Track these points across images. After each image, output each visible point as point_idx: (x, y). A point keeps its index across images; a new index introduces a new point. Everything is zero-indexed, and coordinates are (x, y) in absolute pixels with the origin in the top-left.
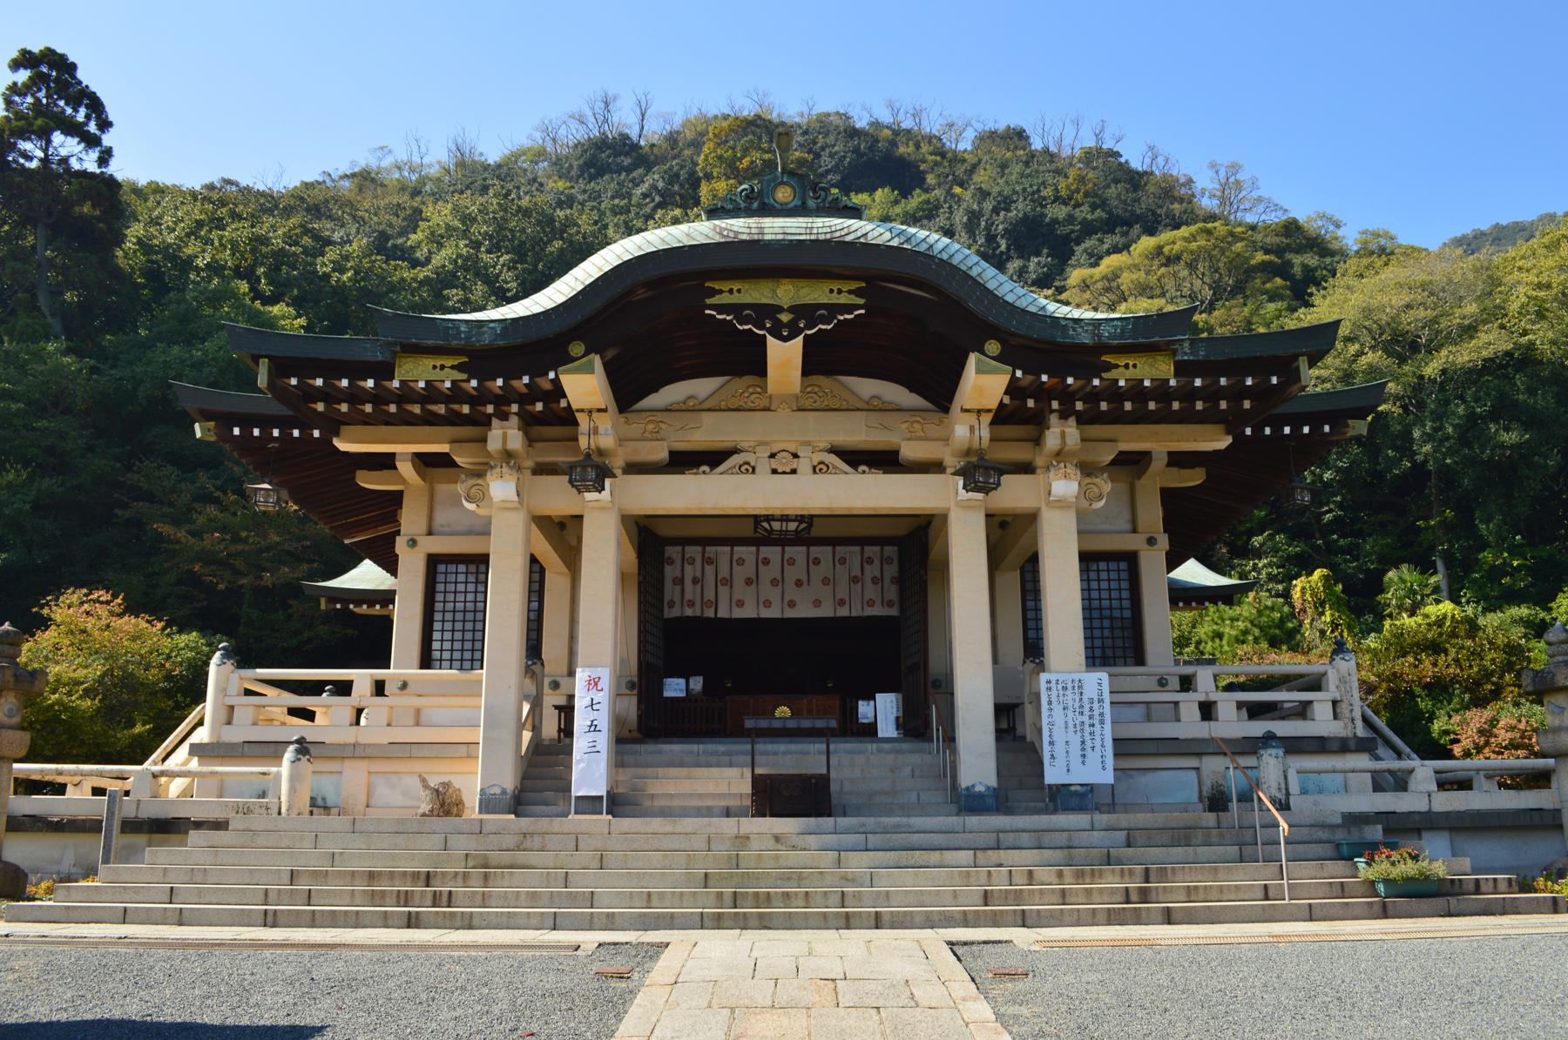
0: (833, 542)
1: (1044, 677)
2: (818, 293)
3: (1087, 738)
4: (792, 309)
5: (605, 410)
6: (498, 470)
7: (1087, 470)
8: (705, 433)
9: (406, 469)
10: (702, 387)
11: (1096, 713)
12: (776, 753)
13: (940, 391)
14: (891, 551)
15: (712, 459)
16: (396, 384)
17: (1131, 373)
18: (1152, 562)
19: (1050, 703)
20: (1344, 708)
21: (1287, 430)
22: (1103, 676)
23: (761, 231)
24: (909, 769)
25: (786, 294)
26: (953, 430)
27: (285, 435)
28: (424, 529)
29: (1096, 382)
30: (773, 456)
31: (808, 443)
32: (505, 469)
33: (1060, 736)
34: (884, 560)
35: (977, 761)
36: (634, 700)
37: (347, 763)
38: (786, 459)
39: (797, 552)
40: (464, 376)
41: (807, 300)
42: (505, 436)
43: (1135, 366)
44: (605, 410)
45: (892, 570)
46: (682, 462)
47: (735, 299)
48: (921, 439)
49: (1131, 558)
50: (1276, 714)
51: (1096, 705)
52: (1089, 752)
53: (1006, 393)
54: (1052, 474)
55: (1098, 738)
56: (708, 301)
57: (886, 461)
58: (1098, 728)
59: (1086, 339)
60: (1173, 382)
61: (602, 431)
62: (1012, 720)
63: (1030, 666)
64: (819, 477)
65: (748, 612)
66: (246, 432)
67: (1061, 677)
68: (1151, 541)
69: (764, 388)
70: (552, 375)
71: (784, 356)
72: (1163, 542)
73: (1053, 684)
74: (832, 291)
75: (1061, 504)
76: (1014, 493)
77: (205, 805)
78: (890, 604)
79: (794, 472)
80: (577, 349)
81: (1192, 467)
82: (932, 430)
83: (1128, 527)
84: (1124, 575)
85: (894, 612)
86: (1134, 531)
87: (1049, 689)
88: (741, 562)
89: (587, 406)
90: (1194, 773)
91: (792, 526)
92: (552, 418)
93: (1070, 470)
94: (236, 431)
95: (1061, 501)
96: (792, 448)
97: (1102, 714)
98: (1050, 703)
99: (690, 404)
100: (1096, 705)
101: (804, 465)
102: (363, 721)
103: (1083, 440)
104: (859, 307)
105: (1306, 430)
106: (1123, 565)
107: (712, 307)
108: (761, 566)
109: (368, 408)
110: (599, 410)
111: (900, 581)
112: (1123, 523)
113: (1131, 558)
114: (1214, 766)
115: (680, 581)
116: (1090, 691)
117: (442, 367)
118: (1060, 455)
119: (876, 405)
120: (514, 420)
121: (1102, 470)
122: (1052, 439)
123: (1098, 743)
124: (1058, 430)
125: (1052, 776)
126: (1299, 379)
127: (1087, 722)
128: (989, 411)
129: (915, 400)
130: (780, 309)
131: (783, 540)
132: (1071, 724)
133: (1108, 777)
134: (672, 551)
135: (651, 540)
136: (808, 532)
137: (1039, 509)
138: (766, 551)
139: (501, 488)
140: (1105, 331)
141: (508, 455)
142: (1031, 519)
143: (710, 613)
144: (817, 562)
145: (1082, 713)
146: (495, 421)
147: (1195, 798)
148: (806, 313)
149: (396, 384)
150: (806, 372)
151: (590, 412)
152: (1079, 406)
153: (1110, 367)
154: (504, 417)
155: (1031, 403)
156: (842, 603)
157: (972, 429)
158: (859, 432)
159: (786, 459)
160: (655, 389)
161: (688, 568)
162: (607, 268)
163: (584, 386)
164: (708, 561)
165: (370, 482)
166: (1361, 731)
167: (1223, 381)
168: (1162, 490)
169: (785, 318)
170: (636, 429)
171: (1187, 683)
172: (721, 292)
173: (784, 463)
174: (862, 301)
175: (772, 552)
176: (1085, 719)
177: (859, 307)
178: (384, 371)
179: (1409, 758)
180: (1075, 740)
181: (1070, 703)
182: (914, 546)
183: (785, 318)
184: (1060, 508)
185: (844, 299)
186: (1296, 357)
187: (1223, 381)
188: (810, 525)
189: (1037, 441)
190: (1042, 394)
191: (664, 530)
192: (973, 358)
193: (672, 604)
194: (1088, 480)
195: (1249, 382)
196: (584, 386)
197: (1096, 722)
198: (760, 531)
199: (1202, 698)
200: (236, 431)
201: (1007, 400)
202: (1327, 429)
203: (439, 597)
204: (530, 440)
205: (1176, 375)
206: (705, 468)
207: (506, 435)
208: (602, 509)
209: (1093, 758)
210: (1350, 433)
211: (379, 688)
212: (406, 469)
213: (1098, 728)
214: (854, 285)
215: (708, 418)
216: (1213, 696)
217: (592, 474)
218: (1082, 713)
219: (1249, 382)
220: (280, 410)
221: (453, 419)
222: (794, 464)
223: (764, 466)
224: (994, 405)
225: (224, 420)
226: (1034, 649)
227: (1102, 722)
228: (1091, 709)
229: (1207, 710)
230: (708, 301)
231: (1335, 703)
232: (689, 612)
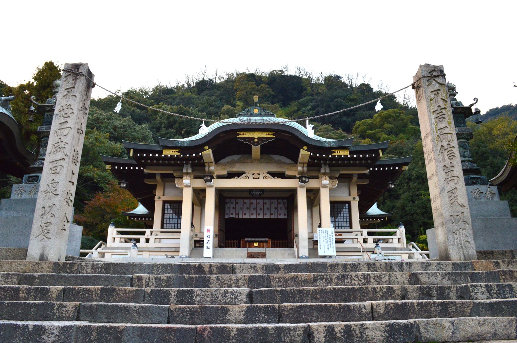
2: (264, 135)
4: (257, 138)
7: (331, 178)
8: (237, 168)
9: (158, 178)
10: (236, 157)
13: (294, 158)
14: (285, 201)
15: (238, 175)
16: (163, 156)
17: (339, 154)
20: (401, 240)
25: (256, 135)
27: (129, 168)
29: (330, 156)
34: (284, 204)
36: (217, 239)
41: (261, 136)
46: (231, 175)
57: (282, 176)
58: (332, 242)
59: (327, 145)
60: (349, 156)
62: (314, 244)
64: (265, 180)
66: (119, 168)
69: (251, 158)
71: (256, 150)
72: (357, 199)
75: (325, 186)
76: (313, 184)
78: (285, 215)
79: (258, 178)
80: (206, 147)
85: (286, 217)
86: (350, 196)
88: (246, 203)
91: (259, 193)
94: (116, 167)
96: (258, 172)
101: (261, 177)
109: (167, 162)
113: (349, 203)
115: (229, 208)
120: (190, 165)
121: (336, 178)
122: (322, 171)
123: (332, 246)
129: (292, 162)
130: (255, 138)
134: (227, 201)
135: (223, 197)
139: (186, 181)
140: (332, 144)
143: (237, 217)
144: (266, 203)
146: (185, 165)
149: (163, 156)
150: (261, 154)
151: (209, 163)
152: (328, 162)
154: (187, 164)
155: (316, 161)
156: (272, 214)
158: (275, 169)
160: (224, 158)
162: (214, 129)
163: (208, 153)
164: (236, 203)
165: (148, 182)
167: (361, 156)
169: (256, 140)
173: (256, 176)
175: (254, 201)
178: (160, 152)
180: (326, 245)
182: (289, 198)
183: (256, 140)
185: (270, 136)
187: (361, 156)
188: (263, 193)
189: (319, 171)
190: (319, 159)
191: (225, 195)
195: (367, 156)
200: (116, 167)
201: (310, 160)
202: (397, 168)
203: (166, 212)
205: (350, 154)
210: (403, 169)
211: (151, 232)
212: (158, 178)
214: (272, 133)
219: (157, 155)
220: (134, 162)
221: (175, 165)
223: (251, 176)
224: (307, 161)
225: (113, 165)
229: (365, 241)
231: (399, 239)
232: (231, 216)
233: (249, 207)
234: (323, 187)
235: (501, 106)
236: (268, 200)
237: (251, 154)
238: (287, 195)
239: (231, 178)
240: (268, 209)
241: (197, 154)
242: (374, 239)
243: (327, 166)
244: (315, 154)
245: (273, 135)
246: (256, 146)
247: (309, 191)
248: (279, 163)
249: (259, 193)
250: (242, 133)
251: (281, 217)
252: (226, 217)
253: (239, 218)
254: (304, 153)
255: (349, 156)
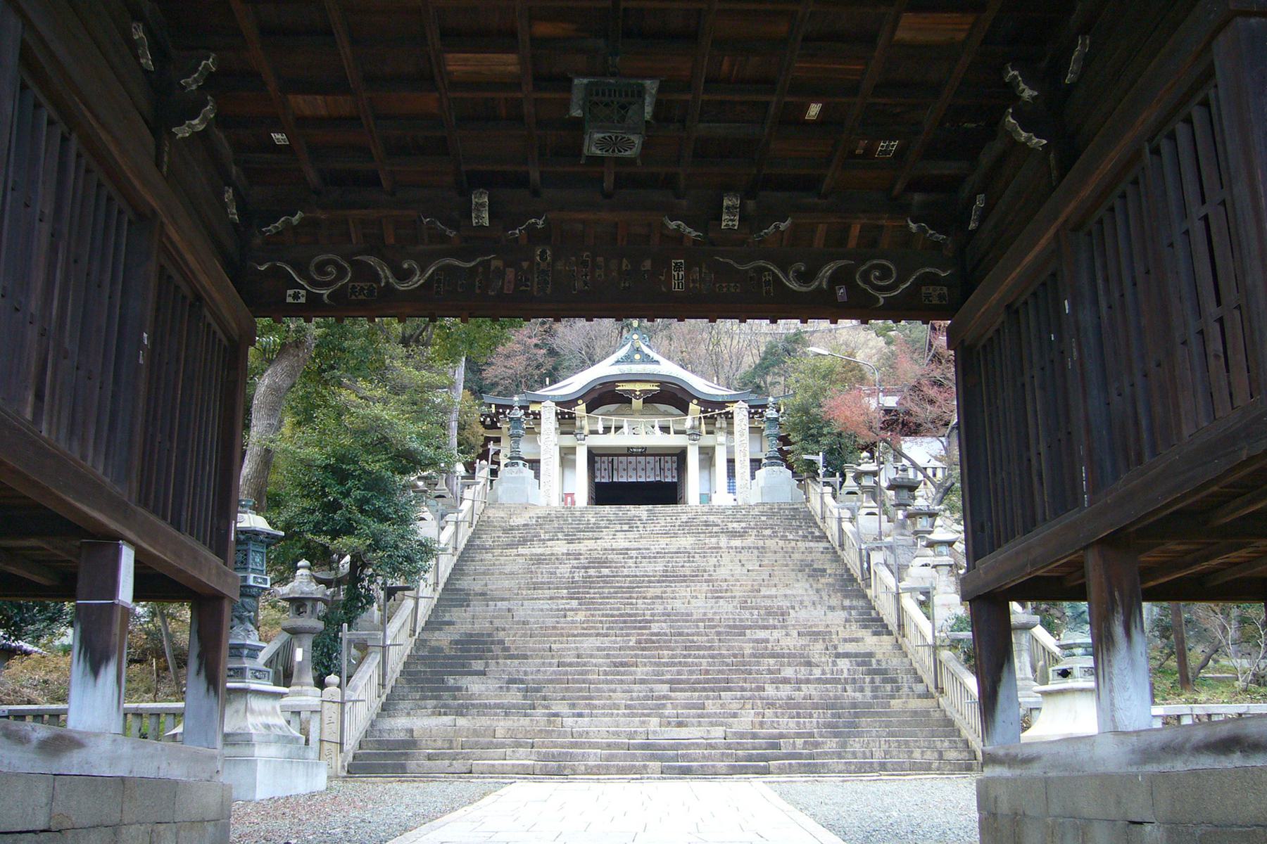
0: (654, 455)
12: (618, 715)
14: (675, 458)
25: (638, 387)
38: (641, 432)
39: (641, 459)
45: (675, 465)
65: (624, 480)
77: (465, 533)
122: (718, 425)
129: (679, 412)
131: (637, 455)
136: (644, 452)
138: (630, 458)
159: (641, 432)
175: (632, 459)
198: (629, 452)
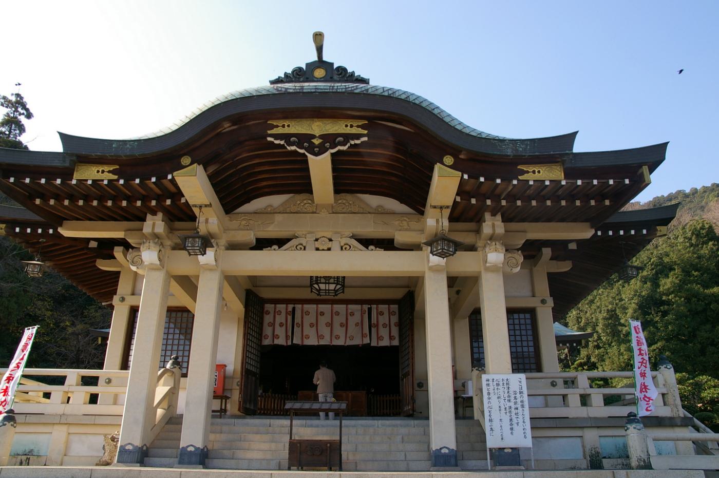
1: (484, 377)
3: (514, 417)
4: (321, 137)
5: (210, 205)
6: (147, 244)
10: (276, 200)
11: (519, 400)
13: (415, 196)
14: (395, 307)
15: (281, 242)
17: (537, 176)
18: (545, 314)
19: (489, 394)
20: (670, 399)
21: (622, 233)
22: (522, 376)
23: (302, 88)
24: (400, 437)
25: (318, 128)
26: (426, 222)
28: (130, 291)
29: (515, 182)
30: (317, 240)
31: (336, 233)
32: (152, 244)
33: (496, 416)
34: (391, 313)
35: (443, 430)
37: (56, 427)
38: (325, 246)
40: (116, 177)
41: (331, 132)
42: (154, 224)
43: (539, 172)
44: (210, 205)
45: (395, 319)
46: (262, 244)
47: (286, 130)
48: (406, 230)
49: (532, 312)
50: (621, 403)
51: (518, 395)
52: (515, 426)
53: (457, 194)
54: (487, 249)
55: (520, 417)
56: (269, 132)
57: (387, 244)
60: (564, 183)
61: (210, 220)
62: (464, 406)
63: (475, 372)
64: (344, 252)
67: (496, 377)
68: (543, 302)
69: (313, 201)
70: (170, 177)
71: (320, 168)
72: (550, 303)
73: (490, 382)
74: (346, 126)
75: (494, 269)
76: (464, 263)
79: (329, 249)
80: (186, 160)
81: (564, 260)
82: (414, 225)
83: (530, 294)
84: (528, 321)
86: (534, 296)
87: (488, 385)
89: (198, 202)
90: (579, 440)
92: (181, 214)
93: (499, 246)
95: (493, 266)
96: (329, 235)
97: (522, 402)
98: (489, 394)
99: (269, 210)
100: (518, 395)
101: (335, 245)
102: (70, 402)
103: (505, 231)
104: (364, 135)
105: (633, 232)
106: (528, 316)
107: (271, 135)
108: (319, 316)
110: (206, 206)
111: (400, 325)
112: (527, 292)
113: (532, 312)
114: (592, 436)
115: (272, 325)
116: (515, 386)
117: (103, 172)
118: (492, 238)
119: (380, 210)
122: (487, 229)
123: (521, 420)
124: (490, 223)
125: (492, 442)
126: (645, 181)
127: (513, 406)
128: (448, 207)
129: (404, 208)
130: (314, 137)
132: (503, 408)
133: (528, 442)
134: (269, 307)
135: (255, 299)
137: (480, 272)
141: (156, 236)
142: (474, 280)
145: (509, 401)
147: (581, 456)
148: (330, 140)
149: (74, 182)
150: (337, 191)
151: (201, 207)
153: (523, 172)
157: (437, 221)
159: (325, 246)
161: (277, 317)
163: (194, 184)
166: (682, 412)
168: (547, 273)
169: (317, 142)
170: (235, 224)
171: (570, 383)
172: (277, 126)
174: (366, 132)
176: (512, 404)
177: (364, 135)
179: (705, 431)
180: (506, 419)
181: (502, 394)
182: (406, 301)
183: (317, 142)
184: (493, 271)
185: (355, 131)
186: (640, 166)
189: (478, 231)
191: (265, 294)
192: (437, 167)
193: (266, 337)
194: (510, 255)
196: (194, 184)
197: (519, 406)
199: (582, 392)
202: (645, 232)
204: (171, 229)
205: (565, 178)
206: (275, 247)
207: (155, 224)
208: (211, 270)
209: (518, 430)
213: (520, 409)
215: (279, 218)
216: (589, 391)
217: (198, 242)
218: (509, 401)
222: (330, 245)
223: (311, 246)
226: (478, 362)
227: (523, 406)
228: (515, 398)
229: (585, 400)
230: (269, 132)
233: (314, 322)
234: (487, 269)
235: (676, 191)
236: (358, 307)
237: (310, 191)
238: (399, 294)
239: (261, 249)
240: (311, 325)
241: (161, 177)
242: (604, 395)
243: (499, 217)
244: (474, 176)
245: (362, 127)
246: (316, 155)
247: (452, 281)
248: (380, 212)
249: (332, 287)
250: (280, 123)
251: (385, 343)
252: (266, 342)
253: (294, 346)
254: (445, 184)
255: (564, 183)
